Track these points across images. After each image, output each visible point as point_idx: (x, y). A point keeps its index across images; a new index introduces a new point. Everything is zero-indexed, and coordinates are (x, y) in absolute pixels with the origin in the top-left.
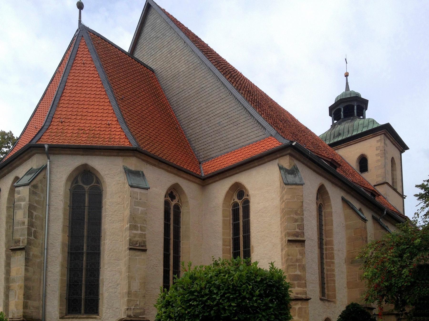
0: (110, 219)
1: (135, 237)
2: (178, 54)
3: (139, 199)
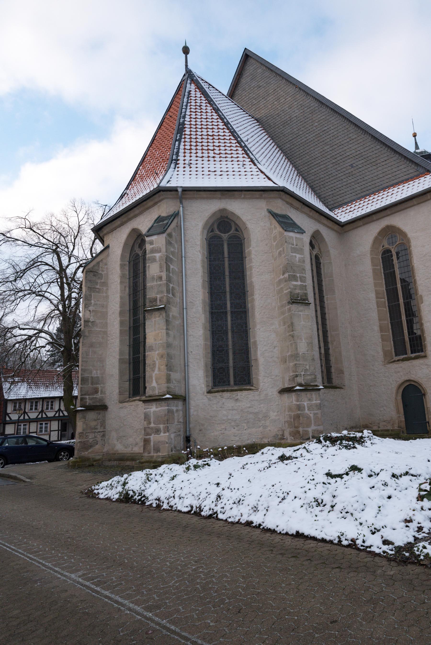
0: (258, 270)
1: (295, 289)
2: (287, 100)
3: (295, 244)
